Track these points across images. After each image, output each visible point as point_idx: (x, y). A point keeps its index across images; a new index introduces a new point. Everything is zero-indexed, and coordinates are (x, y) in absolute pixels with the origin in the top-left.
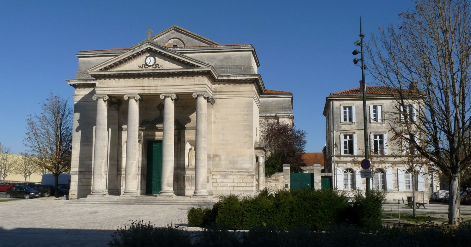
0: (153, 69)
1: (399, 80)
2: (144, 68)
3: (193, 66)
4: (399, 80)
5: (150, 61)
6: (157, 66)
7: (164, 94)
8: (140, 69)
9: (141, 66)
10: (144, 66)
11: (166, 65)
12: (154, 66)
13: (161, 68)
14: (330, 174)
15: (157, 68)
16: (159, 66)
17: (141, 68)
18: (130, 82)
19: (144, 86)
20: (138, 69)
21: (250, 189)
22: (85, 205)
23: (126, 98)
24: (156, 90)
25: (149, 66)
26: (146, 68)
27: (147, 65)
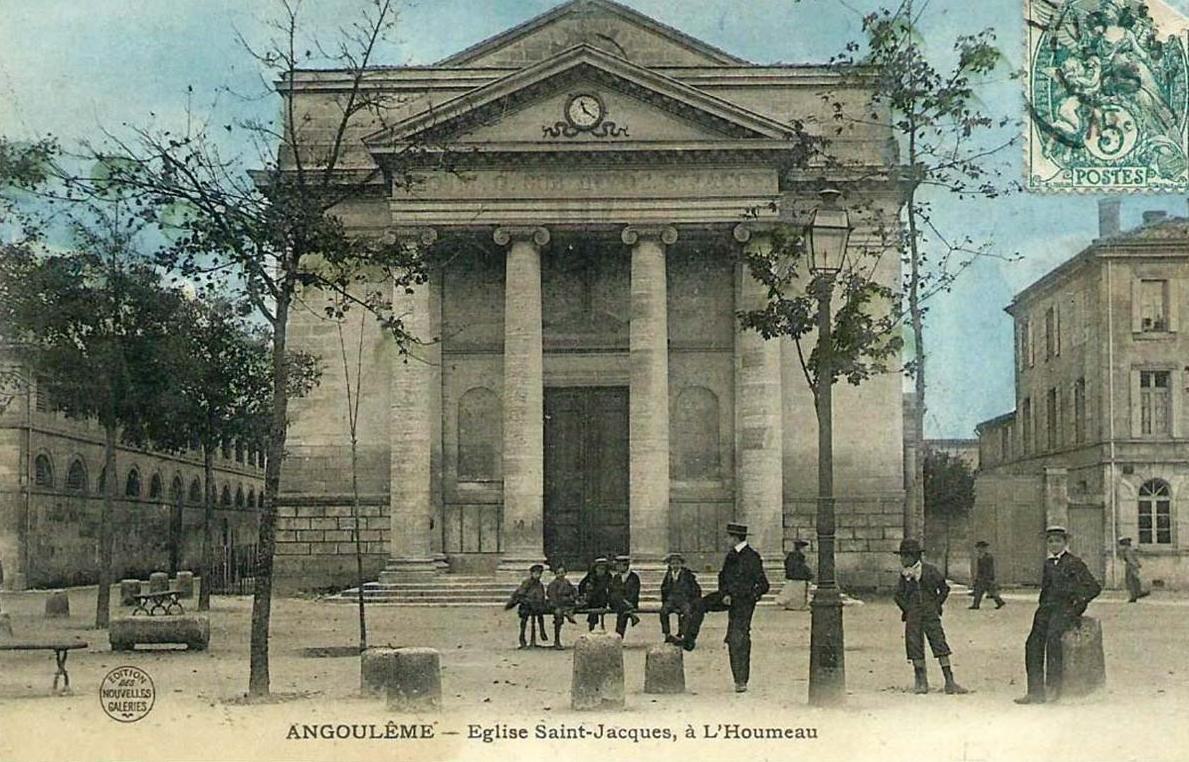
0: (595, 138)
1: (353, 436)
2: (562, 138)
3: (737, 131)
4: (353, 436)
5: (585, 111)
6: (609, 128)
7: (507, 229)
8: (549, 138)
9: (550, 129)
10: (561, 129)
11: (638, 124)
12: (600, 130)
13: (622, 137)
14: (1168, 499)
15: (562, 138)
16: (615, 131)
17: (554, 135)
18: (517, 183)
19: (588, 200)
20: (541, 139)
21: (764, 635)
22: (398, 567)
23: (498, 237)
24: (605, 215)
25: (580, 129)
26: (567, 135)
27: (573, 125)
